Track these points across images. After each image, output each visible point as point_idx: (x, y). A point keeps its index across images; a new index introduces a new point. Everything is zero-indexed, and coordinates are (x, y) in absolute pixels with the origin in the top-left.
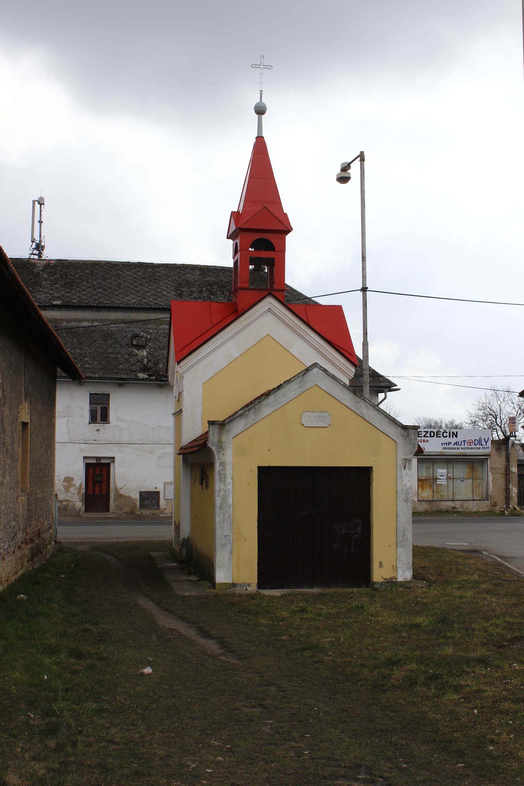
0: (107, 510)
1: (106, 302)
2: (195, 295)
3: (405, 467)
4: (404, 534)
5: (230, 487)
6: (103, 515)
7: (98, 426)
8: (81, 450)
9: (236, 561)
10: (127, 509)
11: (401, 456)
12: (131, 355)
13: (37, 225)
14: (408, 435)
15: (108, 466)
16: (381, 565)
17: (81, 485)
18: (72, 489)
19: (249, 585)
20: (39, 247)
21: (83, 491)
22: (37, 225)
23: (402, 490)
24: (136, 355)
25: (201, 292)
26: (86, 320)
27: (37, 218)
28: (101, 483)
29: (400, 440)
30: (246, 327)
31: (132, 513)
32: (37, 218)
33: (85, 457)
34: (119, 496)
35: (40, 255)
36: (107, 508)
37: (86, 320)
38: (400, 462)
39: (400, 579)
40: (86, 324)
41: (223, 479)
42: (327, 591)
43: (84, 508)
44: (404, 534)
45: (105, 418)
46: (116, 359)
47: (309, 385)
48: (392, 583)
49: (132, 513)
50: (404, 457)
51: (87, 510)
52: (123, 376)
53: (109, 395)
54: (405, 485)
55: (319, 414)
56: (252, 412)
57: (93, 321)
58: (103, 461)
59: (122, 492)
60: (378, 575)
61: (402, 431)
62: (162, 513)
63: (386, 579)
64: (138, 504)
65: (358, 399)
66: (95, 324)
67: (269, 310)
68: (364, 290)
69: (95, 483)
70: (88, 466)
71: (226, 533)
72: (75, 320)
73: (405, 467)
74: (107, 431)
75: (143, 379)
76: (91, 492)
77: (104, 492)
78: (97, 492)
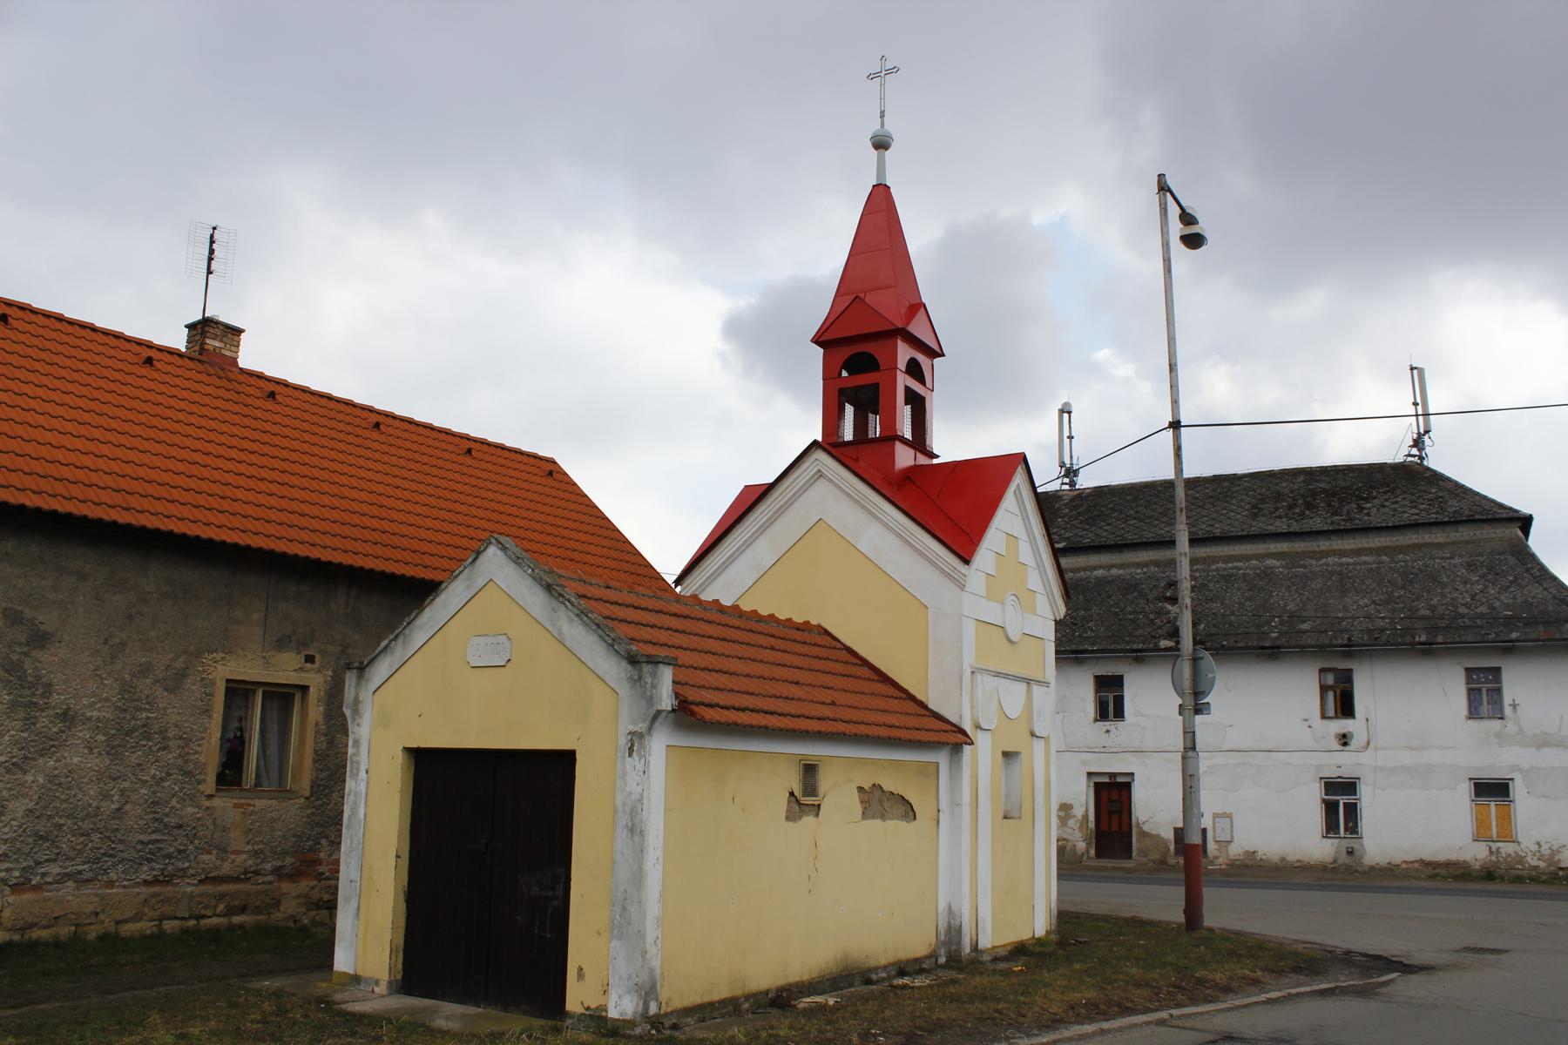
0: (1130, 857)
1: (1130, 537)
2: (1281, 512)
3: (631, 749)
4: (624, 908)
5: (363, 787)
6: (1127, 864)
7: (1107, 725)
8: (1084, 763)
9: (366, 935)
10: (1155, 856)
11: (625, 726)
12: (1159, 613)
13: (1066, 441)
14: (640, 678)
15: (1127, 787)
16: (581, 973)
17: (1086, 816)
18: (1071, 822)
19: (377, 983)
20: (1071, 473)
21: (1092, 825)
22: (1066, 441)
23: (624, 804)
24: (1168, 612)
25: (1291, 507)
26: (1100, 567)
27: (1066, 433)
28: (1120, 812)
29: (624, 689)
30: (783, 510)
31: (1163, 862)
32: (1066, 433)
33: (1089, 774)
34: (1144, 834)
35: (1072, 484)
36: (1127, 853)
37: (1100, 567)
38: (623, 741)
39: (613, 1013)
40: (1099, 573)
41: (355, 775)
42: (1105, 1025)
43: (1092, 852)
44: (624, 908)
45: (1119, 714)
46: (1134, 621)
47: (481, 582)
48: (597, 1019)
49: (1163, 862)
50: (631, 728)
51: (1099, 855)
52: (1135, 646)
53: (1121, 677)
54: (630, 793)
55: (491, 640)
56: (400, 641)
57: (1111, 567)
58: (1119, 780)
59: (1146, 828)
60: (577, 998)
61: (629, 667)
62: (1212, 863)
63: (588, 1009)
64: (1172, 847)
65: (555, 603)
66: (1114, 572)
67: (820, 474)
68: (1175, 425)
69: (1110, 813)
70: (1098, 788)
71: (352, 876)
72: (1085, 569)
73: (631, 749)
74: (1121, 733)
75: (1166, 649)
76: (1104, 828)
77: (1125, 828)
78: (1115, 828)
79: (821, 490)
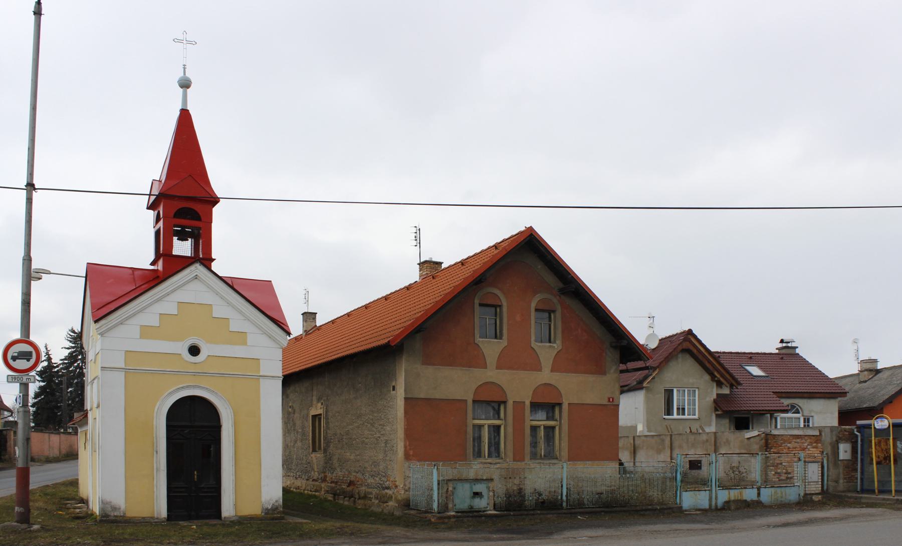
79: (195, 285)
